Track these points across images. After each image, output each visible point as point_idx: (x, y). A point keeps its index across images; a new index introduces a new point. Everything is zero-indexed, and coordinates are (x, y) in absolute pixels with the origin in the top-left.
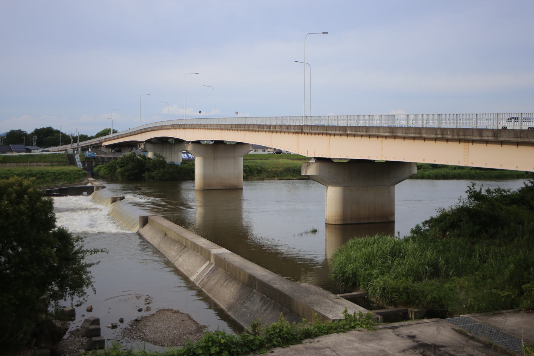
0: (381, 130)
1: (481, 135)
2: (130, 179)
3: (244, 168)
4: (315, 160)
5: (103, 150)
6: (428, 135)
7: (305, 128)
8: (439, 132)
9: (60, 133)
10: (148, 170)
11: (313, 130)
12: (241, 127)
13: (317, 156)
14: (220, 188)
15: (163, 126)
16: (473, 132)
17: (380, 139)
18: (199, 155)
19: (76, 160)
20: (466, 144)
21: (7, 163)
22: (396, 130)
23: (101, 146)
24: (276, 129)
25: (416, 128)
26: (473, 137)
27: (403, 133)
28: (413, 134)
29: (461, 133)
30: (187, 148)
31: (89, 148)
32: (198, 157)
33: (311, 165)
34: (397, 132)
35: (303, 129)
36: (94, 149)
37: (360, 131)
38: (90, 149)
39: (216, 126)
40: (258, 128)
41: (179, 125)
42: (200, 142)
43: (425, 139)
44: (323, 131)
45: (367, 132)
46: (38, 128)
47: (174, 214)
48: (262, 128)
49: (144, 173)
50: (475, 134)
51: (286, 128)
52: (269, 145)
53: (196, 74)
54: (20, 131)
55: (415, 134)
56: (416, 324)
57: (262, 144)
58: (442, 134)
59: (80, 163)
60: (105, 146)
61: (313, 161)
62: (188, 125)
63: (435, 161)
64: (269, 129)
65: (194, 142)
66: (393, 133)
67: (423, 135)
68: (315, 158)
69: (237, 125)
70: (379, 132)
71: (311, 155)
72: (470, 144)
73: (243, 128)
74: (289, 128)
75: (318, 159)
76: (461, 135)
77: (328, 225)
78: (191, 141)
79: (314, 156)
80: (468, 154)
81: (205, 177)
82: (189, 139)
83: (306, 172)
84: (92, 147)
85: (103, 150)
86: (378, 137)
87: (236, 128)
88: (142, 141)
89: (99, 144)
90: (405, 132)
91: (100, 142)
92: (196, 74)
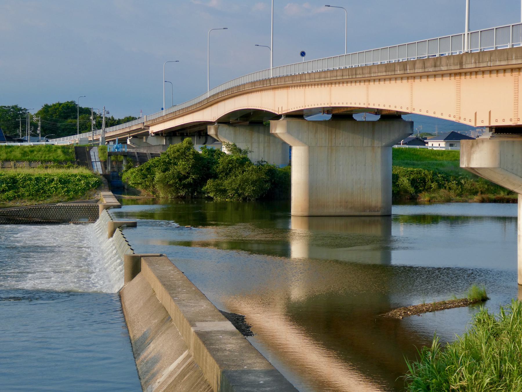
3: (164, 131)
4: (491, 133)
5: (152, 141)
7: (466, 60)
10: (215, 176)
13: (494, 124)
15: (240, 86)
23: (147, 134)
24: (415, 69)
31: (127, 138)
33: (480, 145)
35: (463, 63)
36: (136, 140)
38: (128, 141)
39: (317, 76)
40: (386, 72)
41: (263, 80)
42: (401, 116)
44: (500, 61)
46: (50, 104)
47: (28, 130)
48: (392, 71)
51: (433, 64)
54: (15, 107)
60: (153, 133)
61: (487, 135)
62: (366, 71)
64: (404, 70)
65: (291, 116)
68: (491, 128)
69: (352, 69)
71: (483, 121)
73: (360, 74)
74: (438, 63)
75: (499, 130)
77: (311, 218)
78: (284, 114)
79: (487, 125)
82: (280, 110)
83: (469, 160)
84: (132, 136)
85: (152, 141)
87: (349, 75)
88: (213, 121)
89: (144, 129)
91: (145, 126)
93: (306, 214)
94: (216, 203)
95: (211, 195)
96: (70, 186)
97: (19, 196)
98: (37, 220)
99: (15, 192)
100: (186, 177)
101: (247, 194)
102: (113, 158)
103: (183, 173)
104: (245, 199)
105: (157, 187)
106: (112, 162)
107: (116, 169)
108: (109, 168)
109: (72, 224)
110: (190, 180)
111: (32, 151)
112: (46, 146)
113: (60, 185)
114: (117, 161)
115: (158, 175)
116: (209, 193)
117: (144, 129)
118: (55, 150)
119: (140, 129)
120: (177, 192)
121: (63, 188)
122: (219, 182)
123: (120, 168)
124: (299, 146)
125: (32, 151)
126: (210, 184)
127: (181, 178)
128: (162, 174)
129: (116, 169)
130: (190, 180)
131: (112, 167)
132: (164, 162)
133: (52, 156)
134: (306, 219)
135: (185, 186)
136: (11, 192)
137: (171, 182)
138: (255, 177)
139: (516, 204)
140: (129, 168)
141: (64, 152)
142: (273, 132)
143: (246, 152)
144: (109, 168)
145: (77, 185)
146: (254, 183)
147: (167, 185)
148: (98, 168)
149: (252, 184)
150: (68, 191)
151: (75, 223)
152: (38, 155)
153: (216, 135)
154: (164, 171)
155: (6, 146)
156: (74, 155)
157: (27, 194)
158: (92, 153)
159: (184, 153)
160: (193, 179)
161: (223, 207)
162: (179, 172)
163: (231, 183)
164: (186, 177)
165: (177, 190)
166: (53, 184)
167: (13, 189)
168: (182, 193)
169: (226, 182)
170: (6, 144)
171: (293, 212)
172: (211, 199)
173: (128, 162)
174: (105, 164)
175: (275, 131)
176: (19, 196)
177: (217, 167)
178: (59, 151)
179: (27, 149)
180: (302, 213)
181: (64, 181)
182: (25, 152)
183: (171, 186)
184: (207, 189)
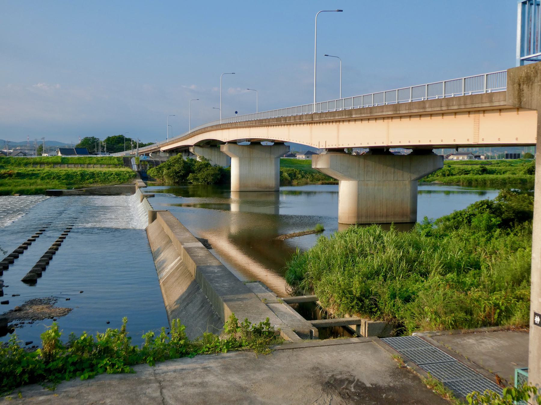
0: (385, 110)
1: (491, 101)
2: (512, 225)
5: (162, 154)
6: (433, 108)
8: (444, 103)
9: (131, 141)
10: (193, 172)
11: (322, 118)
12: (263, 122)
13: (327, 147)
14: (256, 189)
16: (482, 98)
17: (386, 121)
18: (236, 155)
19: (131, 163)
20: (477, 115)
21: (65, 165)
22: (399, 106)
23: (159, 151)
25: (419, 103)
26: (492, 103)
27: (406, 110)
28: (416, 110)
29: (469, 101)
30: (223, 149)
31: (149, 153)
32: (234, 158)
34: (400, 109)
37: (364, 114)
43: (431, 115)
44: (331, 117)
45: (371, 113)
46: (110, 136)
48: (279, 121)
49: (188, 176)
50: (484, 101)
51: (299, 118)
52: (287, 139)
53: (233, 73)
55: (419, 109)
56: (335, 345)
57: (296, 141)
58: (448, 106)
59: (135, 166)
61: (325, 153)
63: (430, 141)
66: (396, 111)
67: (427, 109)
68: (326, 149)
70: (382, 112)
72: (481, 115)
74: (302, 118)
76: (469, 103)
79: (325, 148)
80: (479, 129)
81: (241, 178)
83: (316, 165)
85: (162, 154)
86: (384, 118)
89: (158, 149)
90: (409, 108)
92: (233, 73)
95: (191, 181)
102: (142, 163)
104: (208, 183)
106: (142, 165)
107: (144, 168)
108: (141, 168)
111: (102, 160)
112: (109, 157)
113: (116, 176)
115: (165, 171)
117: (158, 149)
118: (114, 159)
121: (117, 178)
123: (146, 168)
125: (102, 160)
126: (191, 175)
129: (144, 168)
131: (142, 168)
133: (112, 162)
134: (238, 193)
135: (178, 177)
140: (150, 168)
141: (118, 160)
143: (208, 160)
144: (141, 168)
145: (124, 176)
146: (213, 175)
150: (120, 179)
153: (194, 152)
155: (89, 157)
156: (123, 162)
157: (99, 180)
158: (132, 161)
159: (178, 161)
163: (201, 175)
164: (178, 172)
167: (92, 178)
172: (191, 183)
174: (138, 166)
176: (95, 182)
178: (116, 160)
181: (118, 174)
183: (171, 177)
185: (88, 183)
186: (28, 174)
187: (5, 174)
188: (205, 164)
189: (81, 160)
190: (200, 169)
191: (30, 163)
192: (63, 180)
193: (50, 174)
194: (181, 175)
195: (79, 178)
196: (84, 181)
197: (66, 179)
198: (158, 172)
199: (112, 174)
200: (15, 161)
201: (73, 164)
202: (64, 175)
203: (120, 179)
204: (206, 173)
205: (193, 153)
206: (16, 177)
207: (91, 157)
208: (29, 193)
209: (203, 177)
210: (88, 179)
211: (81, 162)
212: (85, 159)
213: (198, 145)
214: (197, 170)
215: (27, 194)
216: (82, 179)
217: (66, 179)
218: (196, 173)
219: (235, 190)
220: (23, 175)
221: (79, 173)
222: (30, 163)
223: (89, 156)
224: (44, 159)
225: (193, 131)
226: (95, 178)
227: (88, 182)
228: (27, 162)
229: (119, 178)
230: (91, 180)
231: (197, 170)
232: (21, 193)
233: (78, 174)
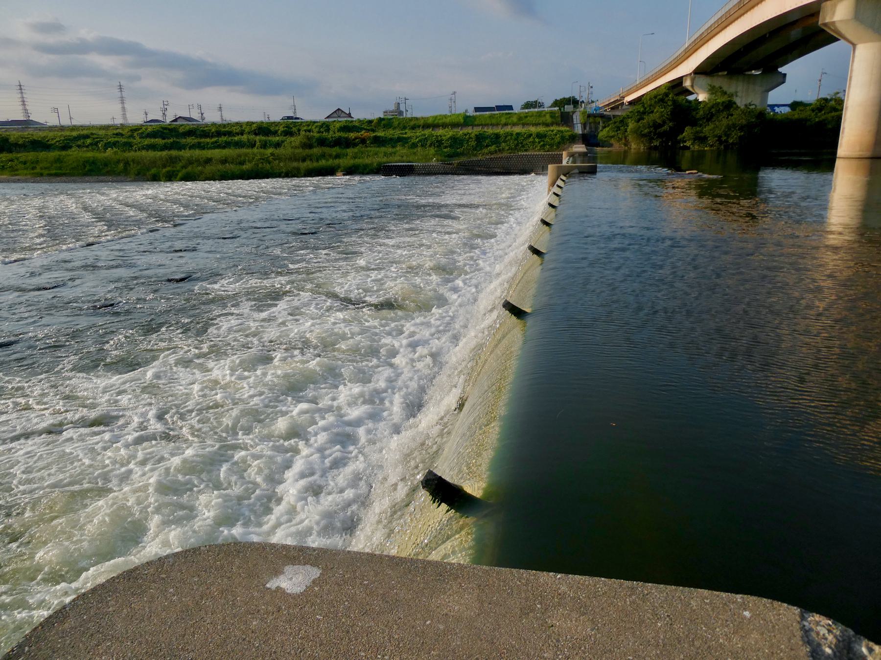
10: (694, 123)
30: (834, 14)
46: (558, 99)
89: (620, 100)
93: (868, 154)
94: (693, 151)
95: (688, 144)
96: (547, 139)
97: (500, 150)
98: (496, 170)
99: (497, 147)
100: (660, 126)
101: (731, 141)
102: (591, 120)
103: (659, 121)
104: (727, 148)
105: (630, 138)
106: (590, 123)
107: (593, 130)
108: (588, 128)
109: (533, 174)
110: (666, 127)
111: (526, 117)
112: (538, 112)
113: (537, 140)
114: (595, 122)
115: (632, 125)
116: (685, 142)
117: (620, 100)
118: (545, 115)
119: (617, 101)
120: (651, 142)
121: (539, 142)
122: (698, 129)
123: (597, 128)
124: (872, 41)
125: (526, 117)
126: (688, 131)
127: (656, 126)
128: (635, 124)
129: (593, 130)
130: (666, 127)
131: (590, 128)
132: (638, 112)
133: (542, 120)
134: (867, 162)
135: (660, 135)
136: (494, 147)
137: (646, 131)
138: (744, 122)
139: (816, 178)
140: (604, 127)
141: (551, 117)
142: (827, 20)
143: (731, 95)
144: (588, 128)
145: (553, 139)
146: (742, 128)
147: (641, 135)
148: (578, 130)
149: (739, 130)
150: (544, 145)
151: (537, 174)
152: (529, 119)
153: (692, 86)
154: (638, 121)
155: (506, 114)
156: (560, 119)
157: (507, 148)
158: (574, 117)
159: (662, 100)
160: (670, 127)
161: (701, 155)
162: (654, 120)
163: (713, 129)
164: (660, 126)
165: (651, 140)
166: (531, 139)
167: (495, 144)
168: (656, 143)
169: (707, 128)
170: (507, 112)
171: (842, 151)
172: (688, 148)
173: (604, 123)
174: (584, 126)
175: (832, 18)
176: (500, 150)
177: (697, 113)
178: (548, 116)
179: (522, 115)
180: (861, 153)
181: (540, 136)
182: (521, 117)
183: (644, 136)
184: (684, 138)
185: (487, 154)
186: (391, 139)
187: (356, 138)
188: (723, 102)
189: (493, 118)
190: (709, 117)
191: (419, 127)
192: (446, 147)
193: (426, 138)
194: (665, 132)
195: (473, 143)
196: (481, 149)
197: (451, 146)
198: (618, 129)
199: (531, 135)
200: (399, 124)
201: (482, 125)
202: (447, 140)
203: (544, 145)
204: (725, 122)
205: (691, 89)
206: (371, 143)
207: (509, 113)
208: (366, 171)
209: (718, 132)
210: (487, 146)
211: (494, 121)
212: (500, 117)
213: (700, 71)
214: (704, 118)
215: (363, 173)
216: (477, 145)
217: (451, 146)
218: (701, 126)
219: (857, 154)
220: (383, 141)
221: (473, 135)
222: (419, 127)
223: (507, 112)
224: (439, 119)
225: (693, 39)
226: (500, 143)
227: (486, 151)
228: (415, 124)
229: (542, 143)
230: (493, 148)
231: (704, 118)
232: (351, 171)
233: (471, 138)
